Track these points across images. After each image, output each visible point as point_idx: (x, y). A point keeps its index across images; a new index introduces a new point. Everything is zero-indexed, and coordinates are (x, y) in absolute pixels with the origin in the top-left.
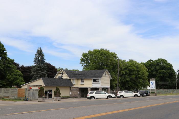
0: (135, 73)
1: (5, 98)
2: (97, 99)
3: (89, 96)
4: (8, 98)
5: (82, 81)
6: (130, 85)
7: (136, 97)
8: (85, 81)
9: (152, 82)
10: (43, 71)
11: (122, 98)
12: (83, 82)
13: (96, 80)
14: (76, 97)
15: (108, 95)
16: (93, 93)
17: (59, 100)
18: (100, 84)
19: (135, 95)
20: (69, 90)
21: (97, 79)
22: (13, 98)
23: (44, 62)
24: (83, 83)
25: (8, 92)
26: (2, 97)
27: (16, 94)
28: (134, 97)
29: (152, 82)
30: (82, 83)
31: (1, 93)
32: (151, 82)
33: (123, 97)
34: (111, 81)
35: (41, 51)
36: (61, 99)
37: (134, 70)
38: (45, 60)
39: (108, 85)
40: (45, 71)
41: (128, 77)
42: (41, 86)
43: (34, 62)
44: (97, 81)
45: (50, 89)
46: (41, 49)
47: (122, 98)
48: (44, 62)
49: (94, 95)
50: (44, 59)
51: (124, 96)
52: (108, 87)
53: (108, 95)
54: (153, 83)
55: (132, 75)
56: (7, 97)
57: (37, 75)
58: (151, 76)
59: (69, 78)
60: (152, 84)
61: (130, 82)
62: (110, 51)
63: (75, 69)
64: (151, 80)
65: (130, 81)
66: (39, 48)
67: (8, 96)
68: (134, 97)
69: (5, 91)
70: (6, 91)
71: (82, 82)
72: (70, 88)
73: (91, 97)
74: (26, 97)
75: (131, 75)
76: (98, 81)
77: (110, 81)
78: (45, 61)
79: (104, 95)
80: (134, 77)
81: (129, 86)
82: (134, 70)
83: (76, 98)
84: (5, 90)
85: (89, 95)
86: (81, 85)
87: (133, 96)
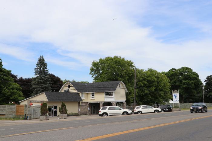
0: (156, 84)
2: (110, 115)
3: (101, 113)
4: (4, 117)
5: (93, 95)
6: (149, 99)
7: (156, 113)
8: (96, 95)
9: (174, 95)
10: (46, 84)
11: (140, 114)
13: (109, 94)
14: (85, 114)
15: (123, 110)
17: (65, 118)
18: (114, 98)
19: (155, 111)
20: (78, 106)
21: (110, 92)
23: (47, 73)
24: (94, 97)
25: (4, 110)
27: (14, 111)
28: (154, 112)
29: (174, 95)
30: (92, 97)
32: (173, 94)
33: (142, 113)
34: (127, 95)
35: (44, 60)
36: (68, 117)
37: (154, 81)
38: (48, 70)
39: (123, 99)
42: (44, 101)
44: (110, 95)
45: (55, 105)
46: (43, 58)
47: (140, 114)
48: (47, 73)
49: (106, 111)
53: (123, 110)
54: (176, 95)
57: (38, 89)
58: (174, 88)
59: (76, 92)
60: (175, 97)
61: (149, 95)
63: (189, 68)
64: (174, 93)
65: (150, 94)
66: (41, 57)
67: (5, 114)
68: (154, 112)
71: (92, 96)
72: (79, 103)
73: (104, 113)
74: (25, 115)
75: (150, 86)
76: (112, 95)
77: (126, 94)
78: (48, 72)
79: (119, 111)
80: (153, 89)
82: (154, 81)
83: (85, 115)
85: (101, 111)
86: (91, 99)
87: (154, 112)
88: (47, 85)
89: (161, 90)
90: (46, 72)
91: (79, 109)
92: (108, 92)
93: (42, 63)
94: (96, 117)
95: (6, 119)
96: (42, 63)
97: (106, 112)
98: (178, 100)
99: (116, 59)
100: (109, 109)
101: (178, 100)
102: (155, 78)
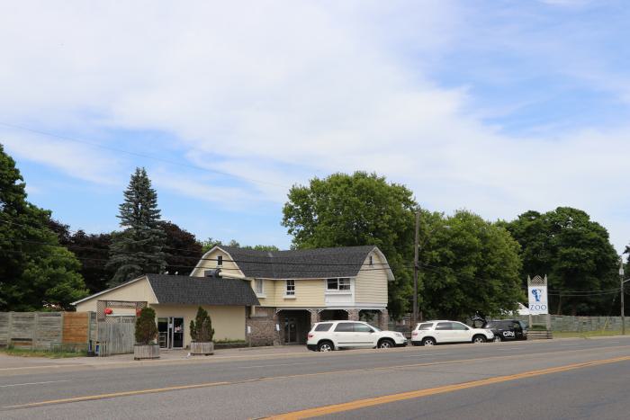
1: (17, 347)
2: (341, 349)
4: (28, 347)
5: (291, 287)
6: (458, 301)
7: (478, 343)
8: (299, 288)
10: (152, 252)
11: (429, 345)
12: (293, 288)
13: (339, 284)
14: (267, 343)
15: (379, 334)
16: (327, 330)
17: (207, 355)
18: (353, 296)
19: (476, 337)
21: (341, 280)
22: (48, 345)
24: (293, 293)
25: (28, 326)
26: (9, 341)
28: (473, 341)
29: (534, 291)
30: (288, 293)
31: (4, 329)
32: (530, 289)
33: (435, 343)
34: (393, 288)
35: (146, 182)
37: (472, 247)
38: (158, 211)
39: (380, 301)
40: (158, 251)
41: (451, 273)
43: (120, 220)
44: (341, 288)
45: (178, 315)
46: (144, 174)
47: (429, 345)
50: (156, 209)
51: (438, 341)
52: (344, 309)
53: (379, 334)
54: (538, 292)
55: (465, 267)
56: (26, 344)
57: (128, 266)
61: (459, 290)
62: (389, 182)
64: (534, 284)
65: (459, 287)
67: (31, 340)
68: (473, 341)
69: (19, 322)
70: (22, 322)
71: (289, 288)
72: (249, 309)
73: (322, 342)
76: (347, 288)
77: (389, 285)
78: (158, 217)
79: (367, 336)
80: (471, 271)
81: (454, 306)
82: (473, 249)
83: (267, 345)
84: (18, 317)
85: (315, 336)
87: (375, 344)
88: (157, 254)
89: (494, 277)
90: (153, 218)
91: (249, 328)
92: (336, 280)
93: (141, 191)
94: (296, 352)
95: (34, 352)
96: (141, 191)
97: (333, 340)
98: (544, 307)
99: (361, 180)
100: (336, 330)
101: (544, 307)
102: (476, 240)
